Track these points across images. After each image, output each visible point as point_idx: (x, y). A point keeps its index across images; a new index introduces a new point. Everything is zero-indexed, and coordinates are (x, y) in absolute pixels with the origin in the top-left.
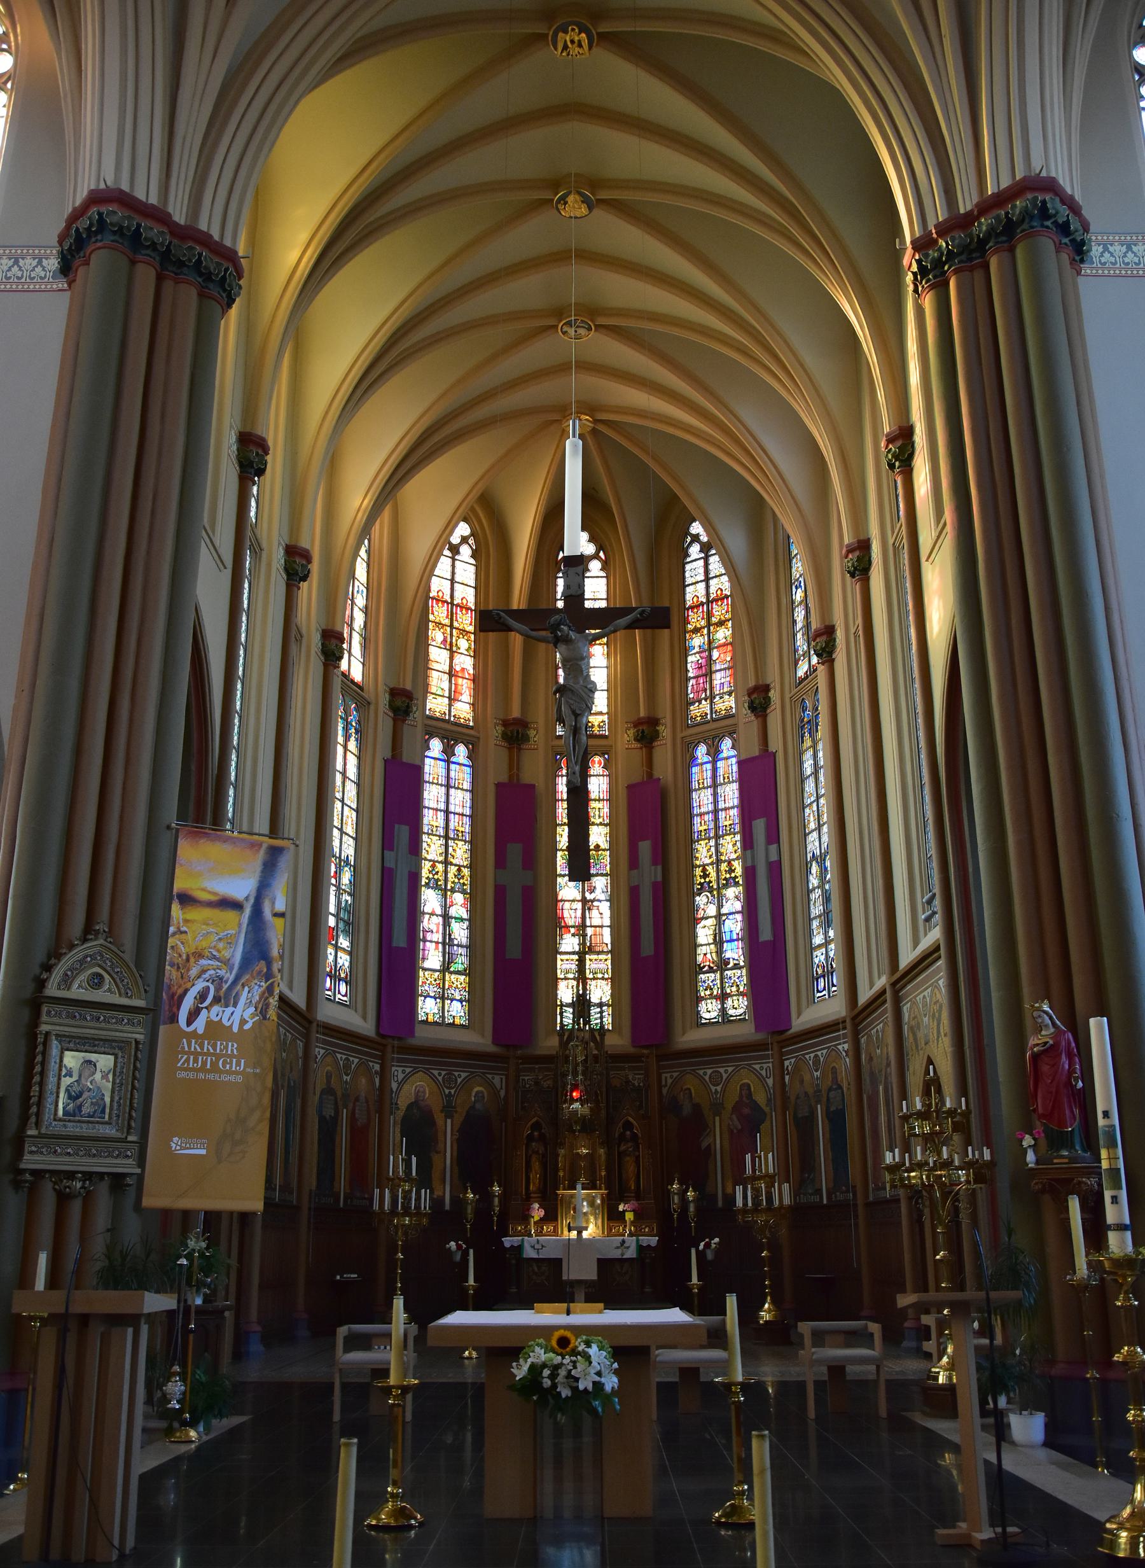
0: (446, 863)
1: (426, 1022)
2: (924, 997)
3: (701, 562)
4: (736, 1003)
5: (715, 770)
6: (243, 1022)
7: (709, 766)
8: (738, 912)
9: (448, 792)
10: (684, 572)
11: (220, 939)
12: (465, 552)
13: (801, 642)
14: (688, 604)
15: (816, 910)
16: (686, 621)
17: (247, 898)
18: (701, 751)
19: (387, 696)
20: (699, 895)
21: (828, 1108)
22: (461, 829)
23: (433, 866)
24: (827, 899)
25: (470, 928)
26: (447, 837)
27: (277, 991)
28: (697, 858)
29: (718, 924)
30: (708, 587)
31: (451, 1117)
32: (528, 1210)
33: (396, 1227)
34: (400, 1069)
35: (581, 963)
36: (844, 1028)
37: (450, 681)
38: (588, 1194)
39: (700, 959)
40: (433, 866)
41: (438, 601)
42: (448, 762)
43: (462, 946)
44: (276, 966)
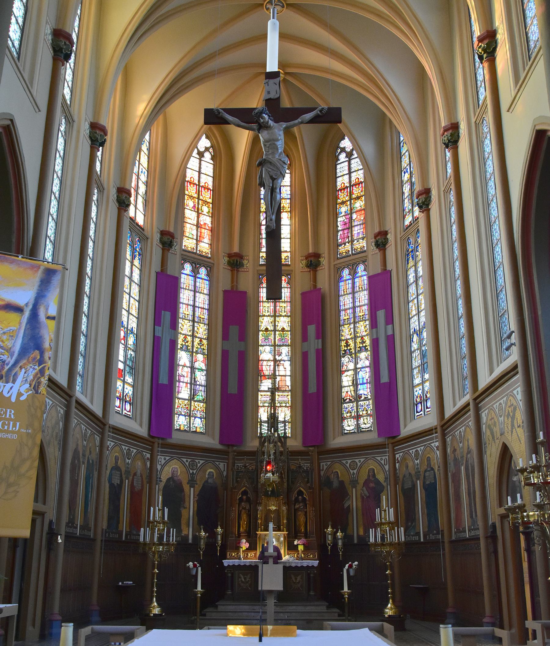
0: (193, 336)
1: (179, 430)
2: (500, 404)
3: (347, 163)
4: (365, 420)
5: (353, 283)
6: (20, 394)
7: (350, 281)
8: (367, 367)
9: (195, 296)
10: (336, 169)
11: (4, 333)
12: (208, 156)
13: (407, 204)
14: (338, 188)
15: (416, 363)
16: (337, 198)
17: (27, 305)
18: (346, 272)
19: (159, 235)
20: (344, 357)
21: (424, 483)
22: (202, 317)
23: (185, 338)
24: (423, 356)
25: (207, 375)
26: (194, 321)
27: (47, 373)
28: (342, 336)
29: (355, 375)
30: (350, 177)
31: (194, 487)
32: (239, 543)
33: (154, 552)
34: (163, 457)
35: (273, 399)
36: (436, 433)
37: (197, 231)
38: (276, 534)
39: (344, 395)
40: (185, 338)
41: (190, 183)
42: (195, 277)
43: (202, 386)
44: (47, 355)
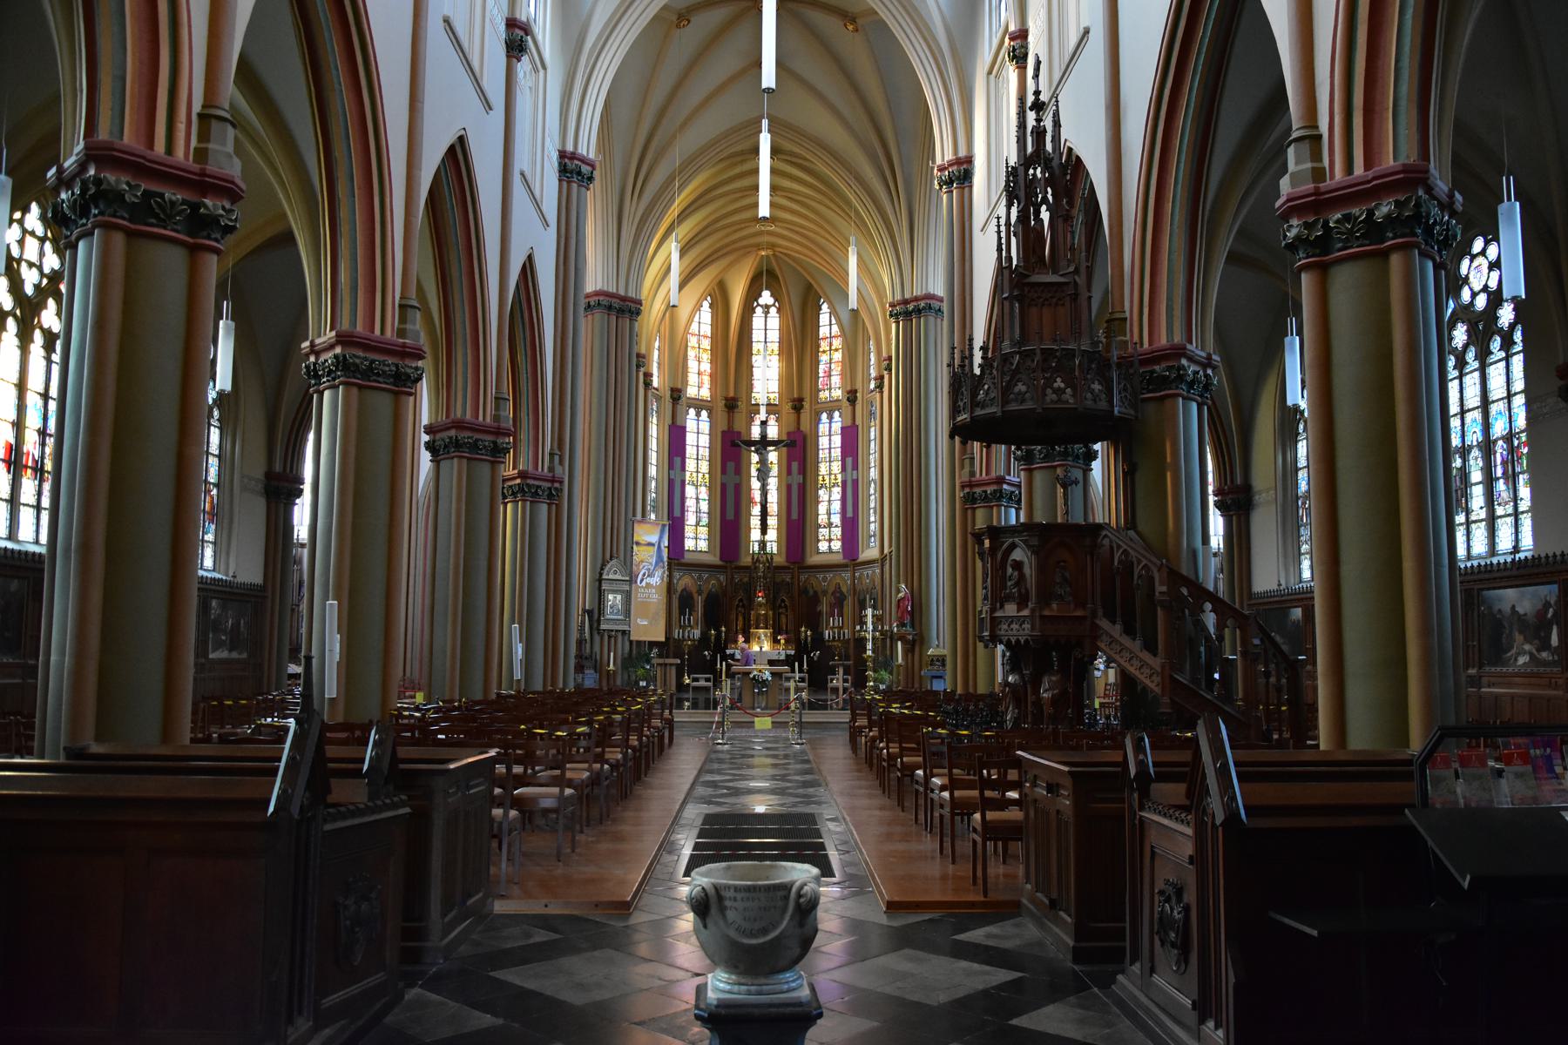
18: (824, 416)
29: (829, 505)
37: (699, 385)
